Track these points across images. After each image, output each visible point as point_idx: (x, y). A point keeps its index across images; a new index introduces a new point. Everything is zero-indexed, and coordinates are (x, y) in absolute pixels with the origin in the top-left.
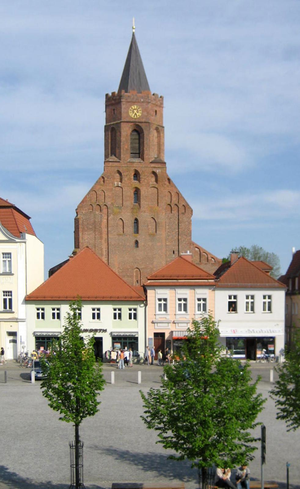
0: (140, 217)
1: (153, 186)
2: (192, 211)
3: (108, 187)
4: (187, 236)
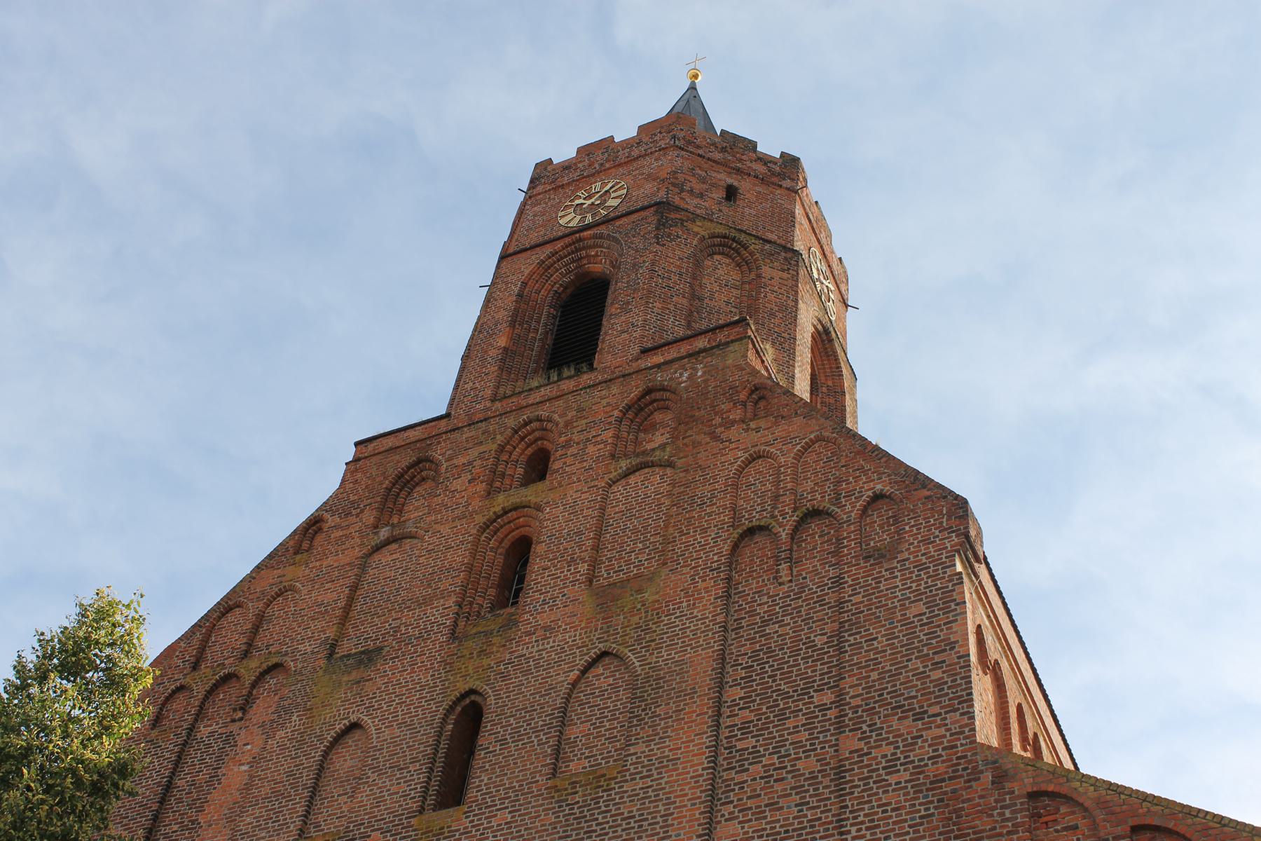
0: (505, 677)
1: (624, 464)
2: (958, 508)
3: (330, 561)
4: (919, 717)
